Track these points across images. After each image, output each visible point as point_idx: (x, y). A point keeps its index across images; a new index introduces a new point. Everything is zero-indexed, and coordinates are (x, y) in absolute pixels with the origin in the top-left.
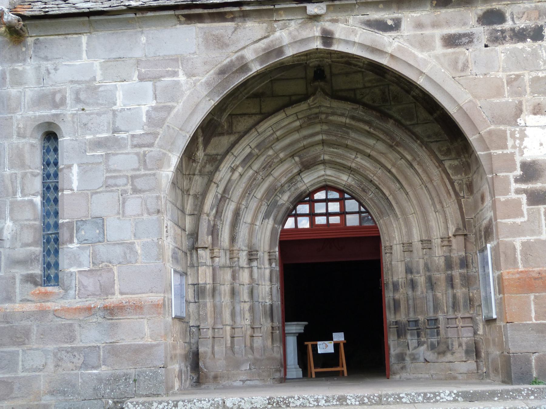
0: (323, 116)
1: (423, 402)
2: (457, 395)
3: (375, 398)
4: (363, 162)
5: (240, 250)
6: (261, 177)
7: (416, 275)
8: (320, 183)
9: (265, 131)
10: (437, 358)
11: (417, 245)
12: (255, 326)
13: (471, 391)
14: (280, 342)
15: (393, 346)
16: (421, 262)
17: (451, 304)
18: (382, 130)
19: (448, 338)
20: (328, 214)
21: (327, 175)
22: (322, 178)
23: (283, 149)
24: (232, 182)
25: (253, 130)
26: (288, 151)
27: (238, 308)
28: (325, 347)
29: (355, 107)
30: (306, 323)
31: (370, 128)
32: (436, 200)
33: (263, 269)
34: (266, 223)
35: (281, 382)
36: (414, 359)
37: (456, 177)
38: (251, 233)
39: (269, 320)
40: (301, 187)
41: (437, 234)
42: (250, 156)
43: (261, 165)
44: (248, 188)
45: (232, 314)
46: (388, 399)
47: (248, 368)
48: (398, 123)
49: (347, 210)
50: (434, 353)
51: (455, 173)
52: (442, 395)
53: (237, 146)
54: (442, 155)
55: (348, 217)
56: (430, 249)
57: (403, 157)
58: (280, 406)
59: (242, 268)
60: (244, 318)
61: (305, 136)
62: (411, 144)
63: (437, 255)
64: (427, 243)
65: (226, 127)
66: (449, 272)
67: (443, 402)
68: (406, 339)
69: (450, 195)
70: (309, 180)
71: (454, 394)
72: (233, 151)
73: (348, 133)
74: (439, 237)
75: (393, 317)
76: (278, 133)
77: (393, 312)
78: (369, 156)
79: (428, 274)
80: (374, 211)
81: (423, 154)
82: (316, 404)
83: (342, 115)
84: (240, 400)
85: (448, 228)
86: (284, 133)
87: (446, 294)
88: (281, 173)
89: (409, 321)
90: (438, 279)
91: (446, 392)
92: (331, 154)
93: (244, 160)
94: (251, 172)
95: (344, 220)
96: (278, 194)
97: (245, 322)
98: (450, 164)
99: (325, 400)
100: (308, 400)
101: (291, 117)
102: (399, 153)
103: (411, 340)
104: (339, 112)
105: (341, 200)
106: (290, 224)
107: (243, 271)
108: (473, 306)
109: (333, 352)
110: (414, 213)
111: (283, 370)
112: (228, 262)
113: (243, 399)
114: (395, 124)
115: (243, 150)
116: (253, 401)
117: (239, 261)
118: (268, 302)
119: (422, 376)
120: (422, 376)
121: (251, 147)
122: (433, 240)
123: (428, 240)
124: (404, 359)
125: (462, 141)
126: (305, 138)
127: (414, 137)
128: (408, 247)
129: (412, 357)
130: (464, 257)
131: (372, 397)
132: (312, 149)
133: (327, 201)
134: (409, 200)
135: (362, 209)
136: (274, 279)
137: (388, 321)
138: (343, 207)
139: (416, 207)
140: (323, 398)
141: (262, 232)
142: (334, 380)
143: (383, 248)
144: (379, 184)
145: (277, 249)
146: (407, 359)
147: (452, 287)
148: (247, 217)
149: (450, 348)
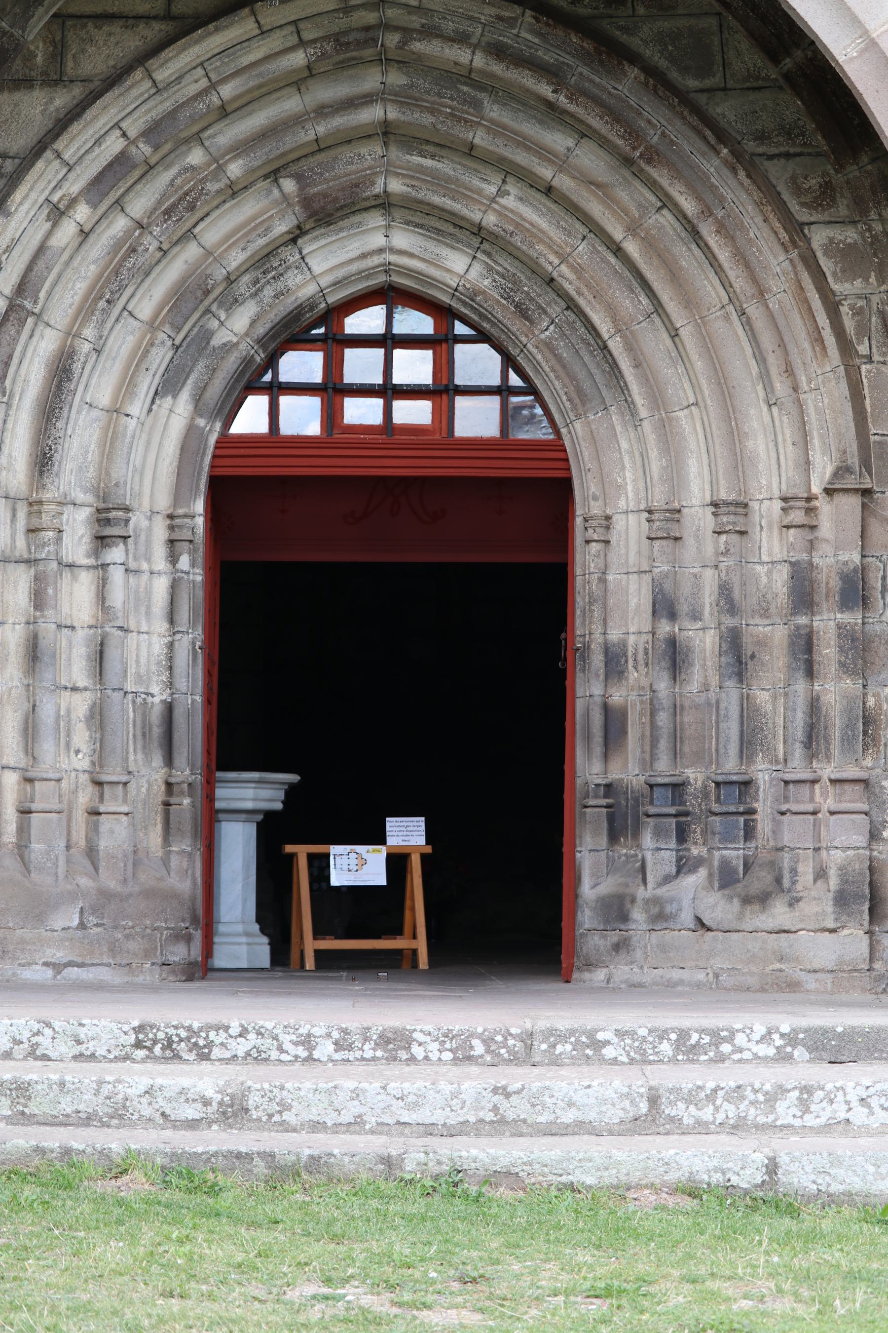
0: (392, 40)
1: (673, 1060)
2: (791, 1039)
3: (511, 1042)
4: (527, 212)
5: (64, 502)
6: (156, 244)
7: (687, 624)
8: (367, 277)
9: (180, 78)
10: (740, 917)
11: (699, 519)
12: (105, 778)
13: (840, 1029)
14: (195, 836)
15: (593, 869)
16: (710, 581)
17: (799, 732)
18: (597, 101)
19: (781, 849)
20: (389, 391)
21: (393, 250)
22: (376, 260)
23: (240, 148)
24: (49, 254)
25: (138, 74)
26: (259, 157)
27: (47, 712)
28: (356, 867)
29: (507, 14)
30: (294, 778)
31: (555, 91)
32: (774, 362)
33: (145, 577)
34: (164, 412)
35: (190, 978)
36: (661, 916)
37: (847, 285)
38: (110, 442)
39: (158, 760)
40: (299, 287)
41: (768, 483)
42: (119, 165)
43: (160, 202)
44: (108, 280)
45: (26, 729)
46: (554, 1046)
47: (76, 922)
48: (658, 81)
49: (460, 379)
50: (730, 898)
51: (843, 271)
52: (740, 1039)
53: (75, 128)
54: (803, 205)
55: (462, 403)
56: (742, 533)
57: (667, 203)
58: (177, 1057)
59: (71, 566)
60: (68, 745)
61: (323, 107)
62: (698, 159)
63: (765, 558)
64: (733, 512)
65: (39, 59)
66: (803, 620)
67: (740, 1061)
68: (639, 846)
69: (824, 348)
70: (328, 262)
71: (782, 1035)
72: (59, 145)
73: (477, 105)
74: (776, 494)
75: (597, 767)
76: (227, 91)
77: (598, 749)
78: (549, 191)
79: (729, 621)
80: (554, 388)
81: (738, 195)
82: (304, 1054)
83: (461, 39)
84: (36, 1027)
85: (808, 462)
86: (249, 91)
87: (786, 695)
88: (229, 231)
89: (651, 786)
90: (762, 643)
91: (754, 1026)
92: (415, 174)
93: (98, 180)
94: (120, 224)
95: (445, 416)
96: (214, 308)
97: (70, 759)
98: (831, 240)
99: (336, 1043)
100: (276, 1038)
101: (278, 34)
102: (653, 185)
103: (655, 851)
104: (449, 26)
105: (441, 344)
106: (252, 417)
107: (75, 578)
108: (875, 741)
109: (384, 883)
111: (198, 935)
112: (21, 542)
113: (48, 1025)
114: (646, 84)
115: (98, 142)
116: (82, 1033)
117: (59, 540)
118: (159, 695)
119: (685, 975)
120: (685, 975)
121: (124, 135)
122: (755, 505)
123: (737, 504)
124: (624, 917)
125: (873, 160)
126: (323, 111)
127: (708, 133)
129: (655, 910)
130: (855, 570)
131: (499, 1038)
132: (347, 152)
133: (388, 341)
134: (682, 356)
135: (515, 380)
136: (184, 614)
137: (579, 781)
138: (444, 366)
139: (704, 383)
140: (329, 1035)
141: (149, 442)
142: (378, 979)
143: (579, 521)
144: (579, 293)
145: (199, 506)
146: (638, 915)
147: (810, 674)
148: (98, 386)
149: (786, 883)
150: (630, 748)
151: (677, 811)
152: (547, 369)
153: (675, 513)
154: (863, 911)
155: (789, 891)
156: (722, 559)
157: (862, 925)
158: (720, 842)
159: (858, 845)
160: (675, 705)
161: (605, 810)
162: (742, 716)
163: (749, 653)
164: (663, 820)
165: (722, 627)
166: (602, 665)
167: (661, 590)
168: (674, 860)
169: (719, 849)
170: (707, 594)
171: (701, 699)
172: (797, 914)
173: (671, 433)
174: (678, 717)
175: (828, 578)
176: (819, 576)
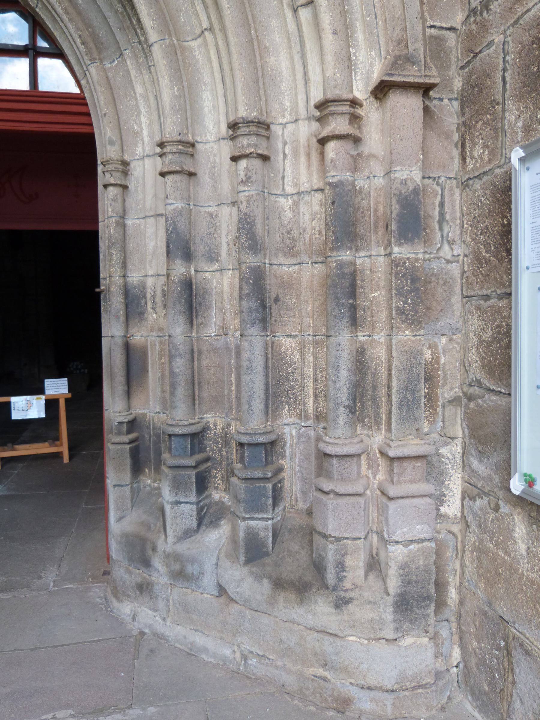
7: (204, 265)
16: (227, 218)
50: (259, 578)
63: (289, 189)
64: (251, 132)
66: (346, 256)
79: (251, 260)
80: (68, 33)
90: (287, 284)
110: (211, 29)
122: (276, 129)
128: (180, 156)
129: (177, 567)
135: (42, 44)
143: (100, 168)
147: (355, 322)
149: (331, 578)
150: (150, 387)
151: (197, 460)
152: (60, 11)
153: (189, 147)
154: (428, 615)
155: (335, 589)
156: (242, 188)
157: (426, 632)
158: (246, 512)
159: (422, 536)
160: (192, 351)
161: (128, 447)
162: (266, 367)
163: (273, 296)
164: (182, 472)
165: (243, 267)
166: (122, 307)
167: (175, 229)
168: (195, 514)
169: (244, 519)
170: (224, 233)
171: (220, 343)
172: (346, 618)
173: (184, 62)
174: (196, 362)
175: (377, 203)
176: (364, 203)
